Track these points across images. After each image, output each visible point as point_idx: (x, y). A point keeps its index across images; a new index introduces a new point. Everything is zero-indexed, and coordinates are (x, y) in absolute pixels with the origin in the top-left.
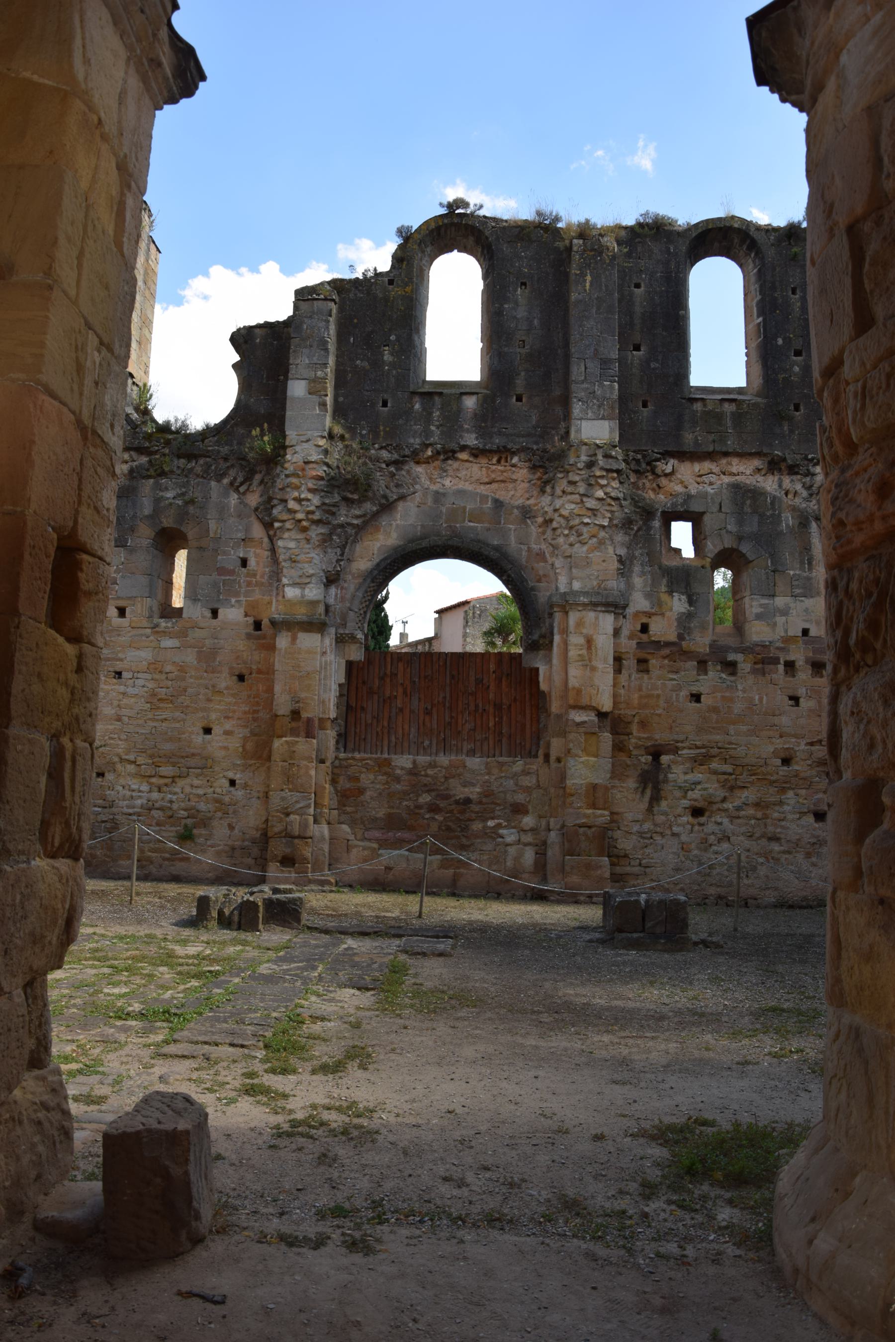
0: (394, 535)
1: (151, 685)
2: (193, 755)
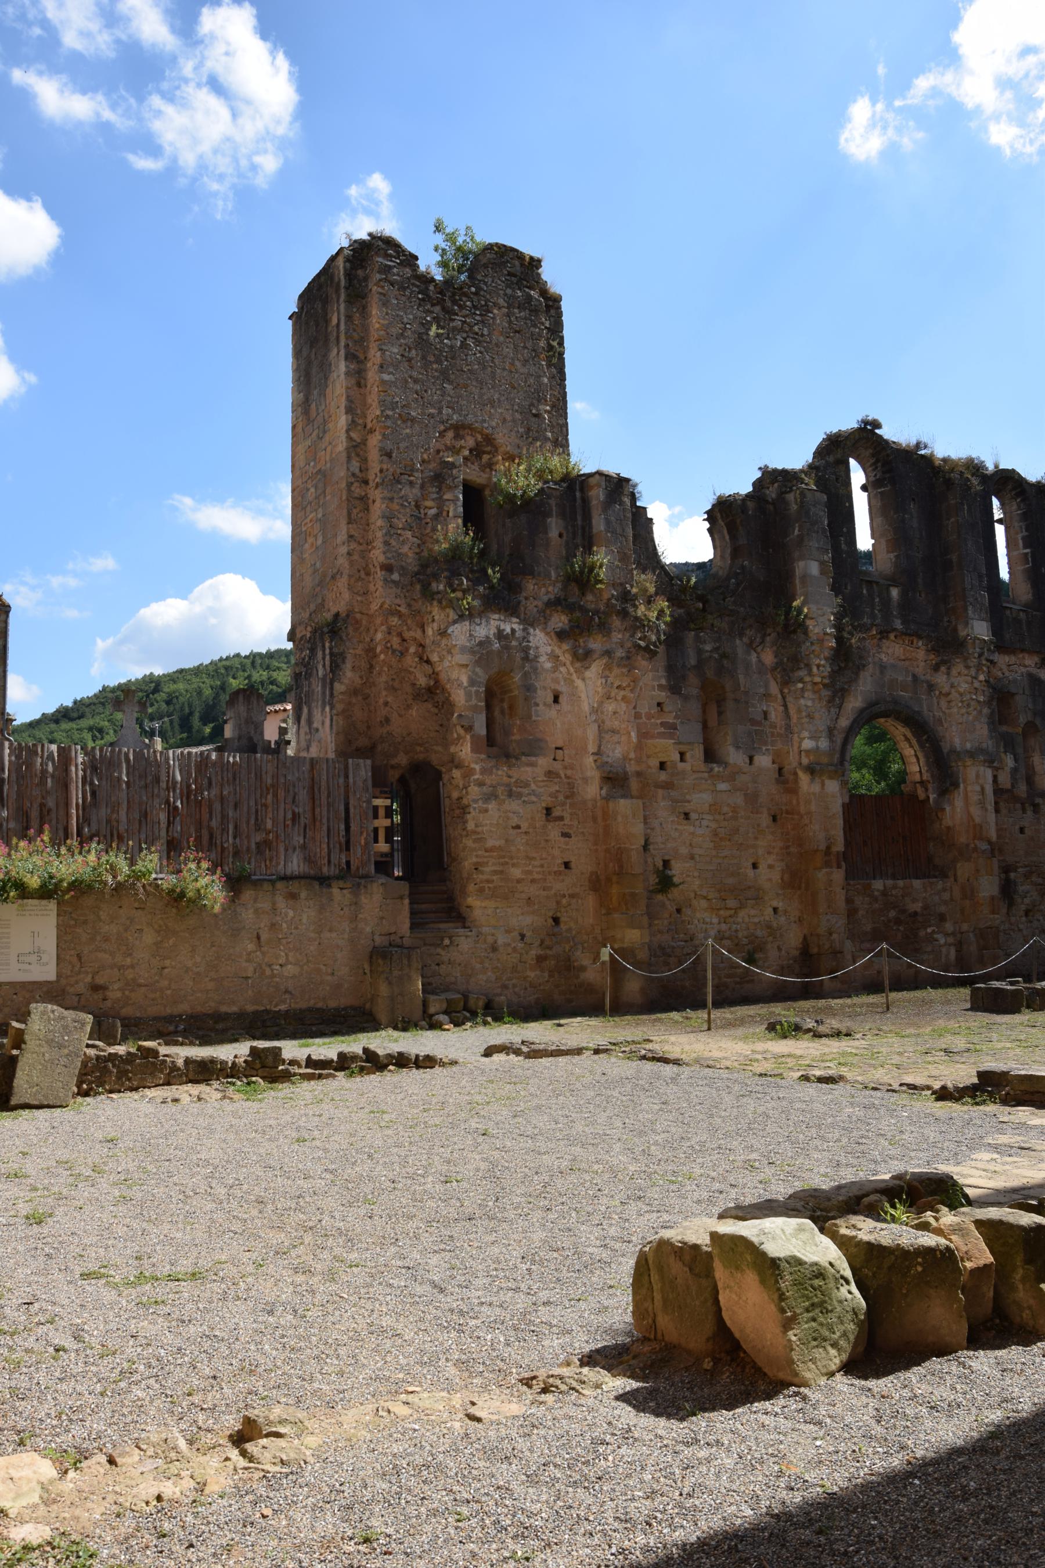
0: (860, 699)
1: (714, 825)
2: (749, 887)
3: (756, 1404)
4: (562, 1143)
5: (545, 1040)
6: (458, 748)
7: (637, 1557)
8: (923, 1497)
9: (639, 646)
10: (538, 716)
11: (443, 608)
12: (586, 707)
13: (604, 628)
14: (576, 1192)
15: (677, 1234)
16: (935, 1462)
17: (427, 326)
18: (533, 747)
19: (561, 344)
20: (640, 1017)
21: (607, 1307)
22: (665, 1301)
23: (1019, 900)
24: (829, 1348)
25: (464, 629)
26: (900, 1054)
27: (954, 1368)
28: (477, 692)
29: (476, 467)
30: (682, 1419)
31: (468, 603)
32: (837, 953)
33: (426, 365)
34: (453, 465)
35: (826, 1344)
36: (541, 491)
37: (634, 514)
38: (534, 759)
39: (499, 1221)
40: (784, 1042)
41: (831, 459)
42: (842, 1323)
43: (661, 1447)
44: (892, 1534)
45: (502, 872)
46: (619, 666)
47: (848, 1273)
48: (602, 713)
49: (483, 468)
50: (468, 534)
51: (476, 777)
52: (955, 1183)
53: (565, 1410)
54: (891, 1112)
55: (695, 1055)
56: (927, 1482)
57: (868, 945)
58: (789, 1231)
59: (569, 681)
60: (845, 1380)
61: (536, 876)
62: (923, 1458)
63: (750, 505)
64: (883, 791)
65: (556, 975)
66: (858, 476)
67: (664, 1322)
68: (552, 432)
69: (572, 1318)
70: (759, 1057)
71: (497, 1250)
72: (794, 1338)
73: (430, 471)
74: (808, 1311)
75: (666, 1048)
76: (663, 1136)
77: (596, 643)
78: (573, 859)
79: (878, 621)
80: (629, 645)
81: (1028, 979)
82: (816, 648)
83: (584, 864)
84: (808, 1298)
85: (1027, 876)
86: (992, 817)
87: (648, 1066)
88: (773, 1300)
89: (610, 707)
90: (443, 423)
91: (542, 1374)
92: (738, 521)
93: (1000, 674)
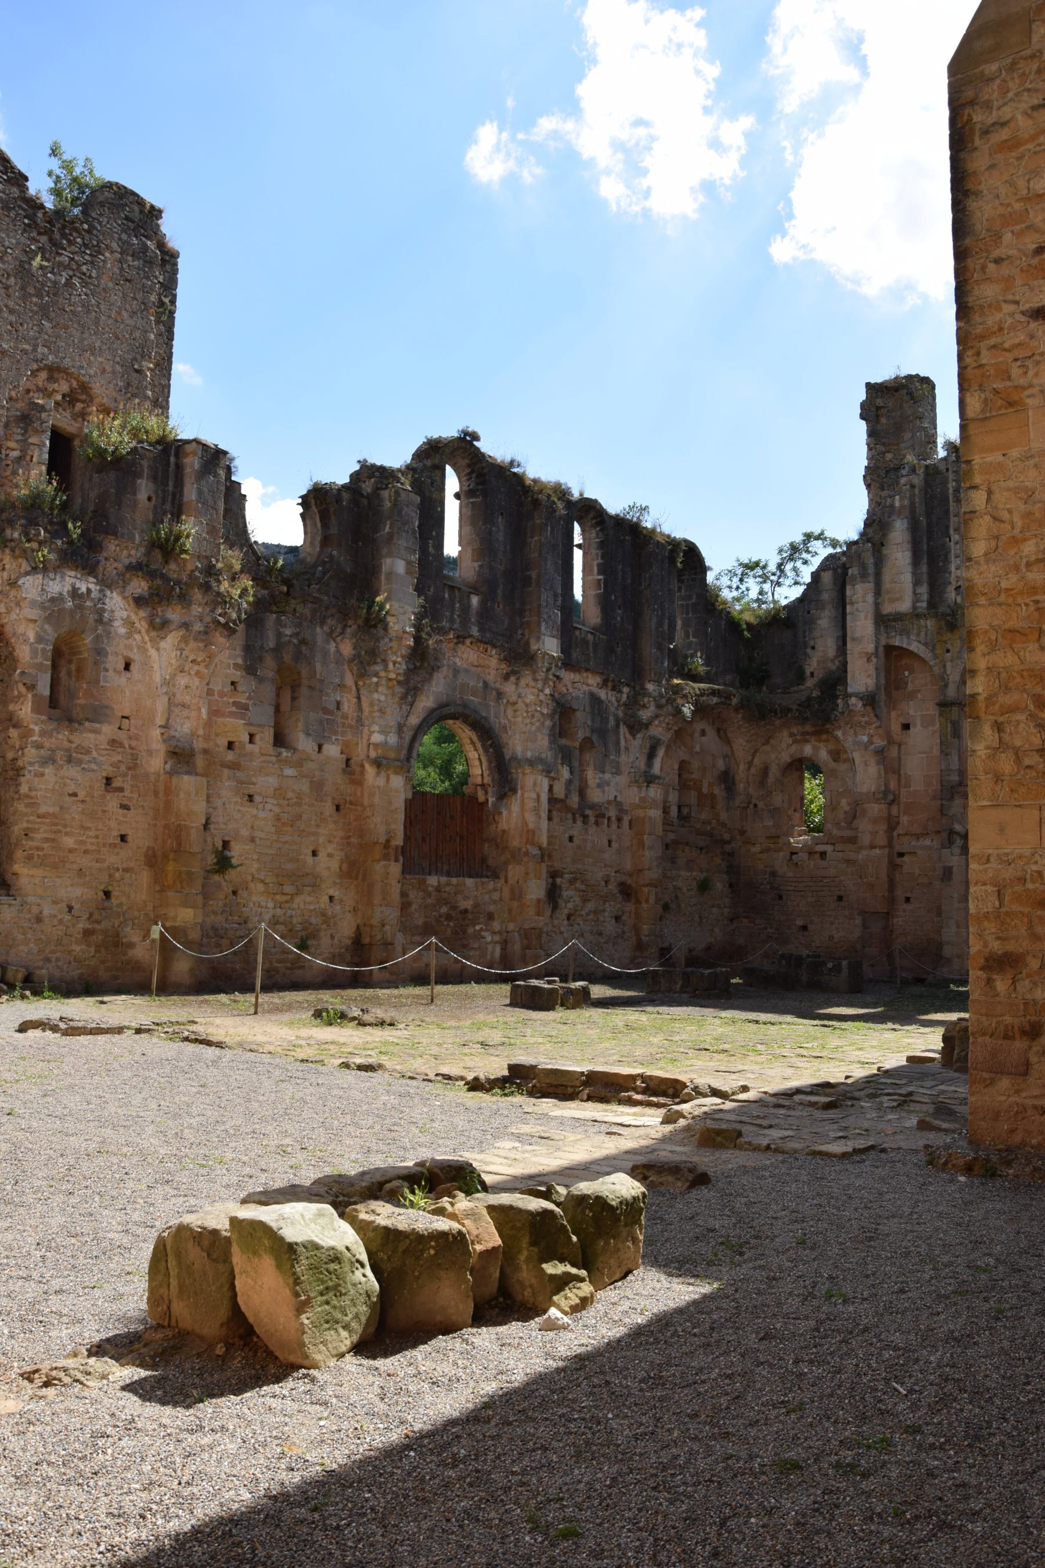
0: (431, 699)
1: (277, 810)
2: (307, 874)
3: (265, 1388)
4: (92, 1124)
5: (85, 1017)
6: (17, 707)
7: (128, 1552)
8: (417, 1467)
9: (219, 622)
10: (106, 682)
11: (15, 558)
12: (157, 678)
13: (184, 599)
14: (102, 1176)
15: (198, 1219)
16: (431, 1434)
17: (31, 255)
18: (98, 714)
19: (173, 302)
20: (187, 998)
21: (123, 1295)
22: (181, 1287)
23: (563, 905)
24: (341, 1330)
25: (36, 583)
26: (439, 1045)
27: (458, 1345)
28: (44, 650)
29: (67, 414)
30: (188, 1407)
31: (43, 556)
32: (387, 944)
33: (25, 297)
34: (42, 408)
35: (339, 1327)
36: (134, 450)
37: (227, 488)
38: (98, 725)
39: (16, 1206)
40: (329, 1029)
41: (429, 463)
42: (355, 1305)
43: (164, 1436)
44: (383, 1505)
45: (53, 840)
46: (195, 639)
47: (364, 1257)
48: (174, 686)
49: (75, 417)
50: (51, 483)
51: (35, 738)
52: (473, 1170)
53: (67, 1404)
54: (425, 1100)
55: (239, 1039)
56: (421, 1453)
57: (417, 938)
58: (308, 1216)
59: (143, 650)
60: (354, 1360)
61: (89, 847)
62: (420, 1431)
63: (346, 496)
64: (447, 790)
65: (103, 950)
66: (452, 483)
67: (179, 1308)
68: (153, 392)
69: (84, 1306)
70: (303, 1043)
71: (10, 1237)
72: (306, 1322)
73: (17, 410)
74: (322, 1294)
75: (210, 1030)
76: (198, 1119)
77: (174, 614)
78: (130, 832)
79: (456, 626)
80: (208, 619)
81: (564, 979)
82: (394, 644)
83: (141, 839)
84: (323, 1282)
85: (572, 882)
86: (544, 824)
87: (190, 1047)
88: (288, 1284)
89: (182, 681)
90: (37, 361)
91: (45, 1367)
92: (332, 510)
93: (564, 690)
